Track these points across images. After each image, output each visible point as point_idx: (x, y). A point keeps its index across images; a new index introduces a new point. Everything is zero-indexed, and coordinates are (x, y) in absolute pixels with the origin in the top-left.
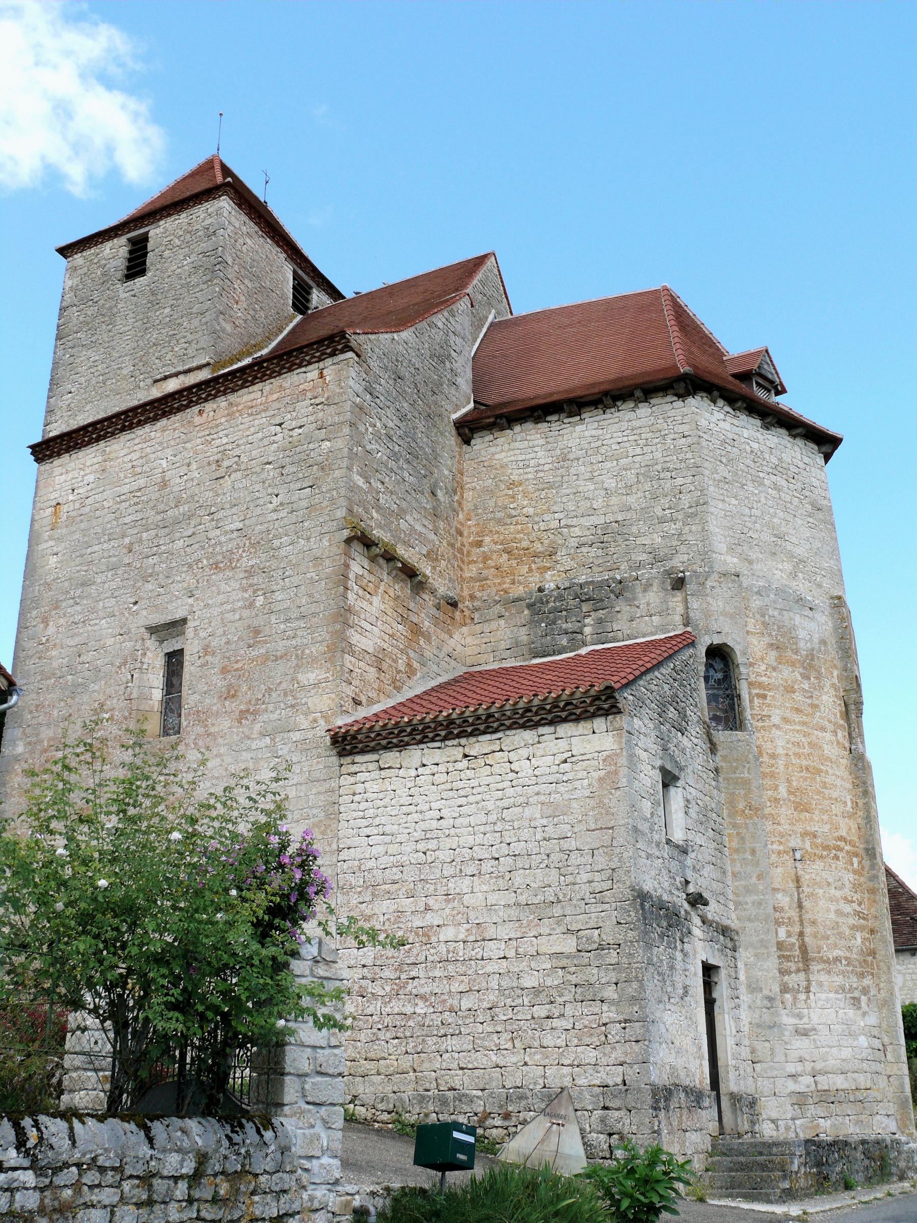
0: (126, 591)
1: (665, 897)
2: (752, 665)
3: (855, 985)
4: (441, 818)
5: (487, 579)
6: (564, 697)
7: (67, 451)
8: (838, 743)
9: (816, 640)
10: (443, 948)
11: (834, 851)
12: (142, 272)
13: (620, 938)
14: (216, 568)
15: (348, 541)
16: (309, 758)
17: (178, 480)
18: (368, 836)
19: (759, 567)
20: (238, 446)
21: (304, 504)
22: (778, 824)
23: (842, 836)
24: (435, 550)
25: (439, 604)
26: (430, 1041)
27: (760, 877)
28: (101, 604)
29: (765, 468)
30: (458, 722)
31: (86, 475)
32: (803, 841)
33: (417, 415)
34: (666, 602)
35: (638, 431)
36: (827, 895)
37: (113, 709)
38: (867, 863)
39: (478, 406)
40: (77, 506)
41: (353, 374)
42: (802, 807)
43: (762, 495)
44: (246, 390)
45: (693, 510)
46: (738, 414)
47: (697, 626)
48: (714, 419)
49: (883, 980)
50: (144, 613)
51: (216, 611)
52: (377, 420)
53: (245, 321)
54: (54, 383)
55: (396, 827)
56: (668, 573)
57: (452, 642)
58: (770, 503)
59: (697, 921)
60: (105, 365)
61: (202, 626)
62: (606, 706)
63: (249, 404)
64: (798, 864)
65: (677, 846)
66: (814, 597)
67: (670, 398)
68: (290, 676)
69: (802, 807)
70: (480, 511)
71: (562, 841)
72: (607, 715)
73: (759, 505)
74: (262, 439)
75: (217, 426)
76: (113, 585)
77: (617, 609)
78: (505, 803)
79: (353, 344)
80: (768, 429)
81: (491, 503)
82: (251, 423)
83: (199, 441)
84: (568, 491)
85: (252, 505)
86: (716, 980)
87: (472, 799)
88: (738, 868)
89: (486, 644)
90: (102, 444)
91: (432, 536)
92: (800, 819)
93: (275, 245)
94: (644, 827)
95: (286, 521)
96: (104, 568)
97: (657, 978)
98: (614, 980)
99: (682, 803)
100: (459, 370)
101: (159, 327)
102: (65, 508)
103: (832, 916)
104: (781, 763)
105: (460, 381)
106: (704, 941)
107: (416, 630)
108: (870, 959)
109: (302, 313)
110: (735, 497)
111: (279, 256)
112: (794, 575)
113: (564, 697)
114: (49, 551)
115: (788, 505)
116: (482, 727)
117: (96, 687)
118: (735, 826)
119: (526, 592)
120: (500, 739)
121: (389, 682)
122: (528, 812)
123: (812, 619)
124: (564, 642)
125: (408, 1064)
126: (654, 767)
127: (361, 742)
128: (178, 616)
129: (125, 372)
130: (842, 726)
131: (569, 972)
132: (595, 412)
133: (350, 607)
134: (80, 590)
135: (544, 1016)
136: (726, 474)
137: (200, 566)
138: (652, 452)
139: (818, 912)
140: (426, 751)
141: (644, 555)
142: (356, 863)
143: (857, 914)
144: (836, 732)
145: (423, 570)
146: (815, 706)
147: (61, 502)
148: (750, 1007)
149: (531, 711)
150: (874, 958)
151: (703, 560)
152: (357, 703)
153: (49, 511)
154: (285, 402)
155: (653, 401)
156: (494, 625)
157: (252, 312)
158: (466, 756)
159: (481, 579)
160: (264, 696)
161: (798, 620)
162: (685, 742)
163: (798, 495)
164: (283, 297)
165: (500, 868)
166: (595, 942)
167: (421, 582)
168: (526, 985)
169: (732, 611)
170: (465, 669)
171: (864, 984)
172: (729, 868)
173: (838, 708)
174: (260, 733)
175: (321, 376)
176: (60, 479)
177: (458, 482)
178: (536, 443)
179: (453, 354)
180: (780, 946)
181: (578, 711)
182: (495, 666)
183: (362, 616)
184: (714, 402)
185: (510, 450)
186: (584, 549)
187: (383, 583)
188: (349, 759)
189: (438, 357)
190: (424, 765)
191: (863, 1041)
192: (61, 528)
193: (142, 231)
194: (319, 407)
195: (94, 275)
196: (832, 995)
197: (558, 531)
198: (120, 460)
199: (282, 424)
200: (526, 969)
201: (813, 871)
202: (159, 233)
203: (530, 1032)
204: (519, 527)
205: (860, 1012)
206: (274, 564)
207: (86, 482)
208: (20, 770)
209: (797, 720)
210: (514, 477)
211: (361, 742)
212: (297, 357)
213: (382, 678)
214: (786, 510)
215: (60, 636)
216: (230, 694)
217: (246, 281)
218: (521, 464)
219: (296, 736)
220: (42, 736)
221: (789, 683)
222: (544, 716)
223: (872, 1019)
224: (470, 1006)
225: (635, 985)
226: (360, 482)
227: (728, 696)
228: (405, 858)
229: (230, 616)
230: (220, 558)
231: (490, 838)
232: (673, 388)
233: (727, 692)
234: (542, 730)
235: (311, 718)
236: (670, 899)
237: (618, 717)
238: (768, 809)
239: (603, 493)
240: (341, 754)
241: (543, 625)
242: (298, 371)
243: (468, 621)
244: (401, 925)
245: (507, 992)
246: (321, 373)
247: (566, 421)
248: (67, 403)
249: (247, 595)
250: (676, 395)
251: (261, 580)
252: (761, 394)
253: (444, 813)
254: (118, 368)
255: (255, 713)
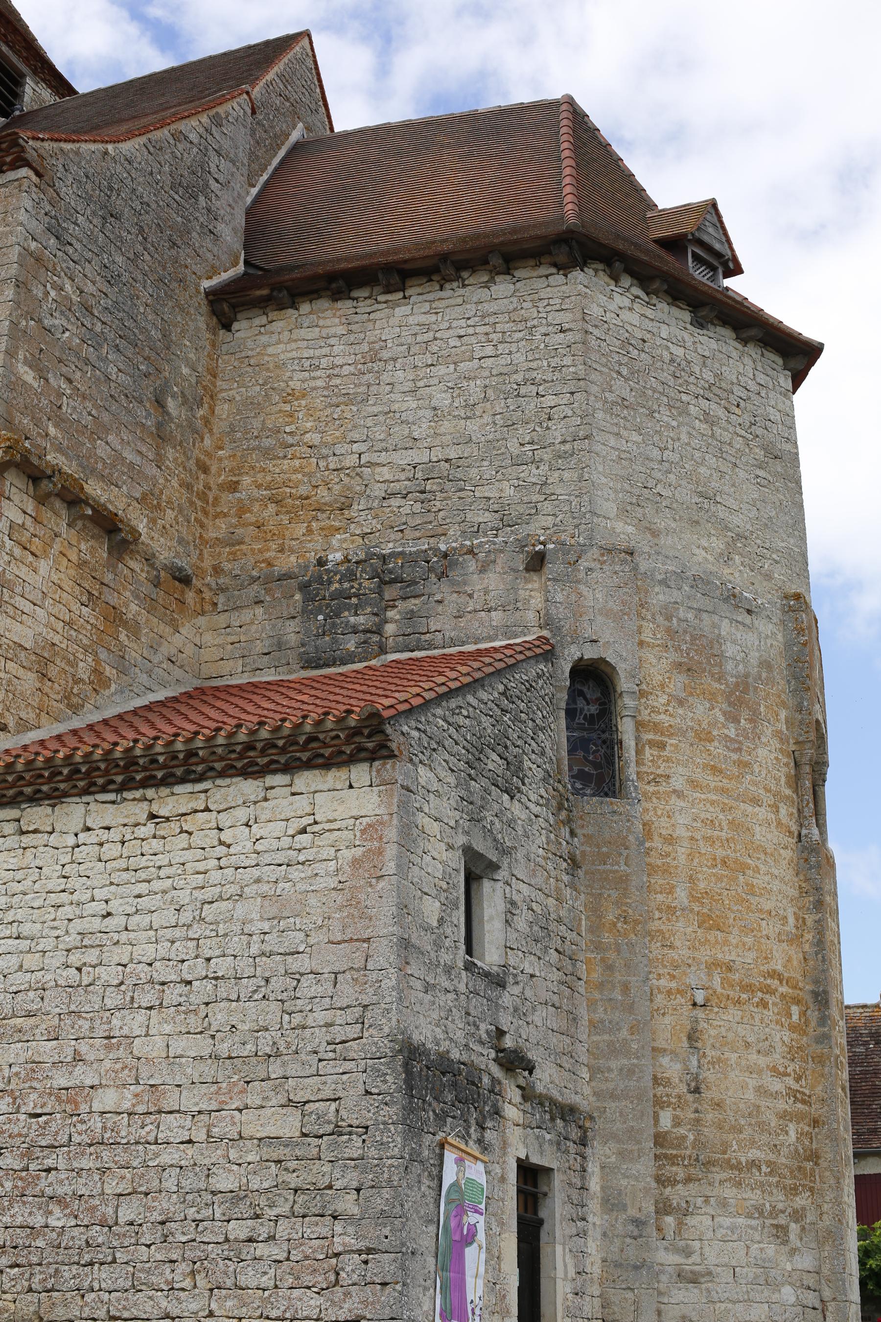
1: (455, 1055)
2: (642, 694)
3: (780, 1206)
4: (109, 914)
5: (241, 543)
6: (308, 728)
8: (779, 823)
9: (754, 662)
10: (96, 1123)
11: (760, 994)
13: (368, 1118)
19: (669, 542)
22: (671, 947)
23: (774, 971)
24: (157, 492)
25: (158, 577)
26: (67, 1272)
27: (632, 1030)
29: (692, 388)
30: (141, 761)
32: (709, 975)
33: (140, 277)
34: (515, 590)
35: (492, 320)
36: (744, 1062)
38: (813, 1015)
41: (28, 204)
42: (711, 922)
43: (684, 429)
45: (568, 447)
46: (654, 300)
47: (559, 629)
48: (613, 307)
49: (827, 1199)
52: (66, 280)
55: (38, 926)
56: (521, 545)
58: (695, 443)
59: (514, 1094)
62: (370, 745)
64: (700, 1013)
65: (487, 975)
66: (756, 593)
67: (544, 270)
69: (711, 922)
70: (239, 435)
71: (290, 959)
72: (373, 760)
73: (677, 444)
77: (438, 597)
78: (209, 893)
79: (31, 155)
80: (702, 326)
81: (256, 424)
84: (376, 409)
86: (545, 1189)
87: (157, 885)
88: (600, 1014)
89: (236, 646)
92: (707, 940)
94: (425, 941)
97: (428, 1183)
98: (355, 1184)
99: (501, 906)
100: (222, 212)
103: (750, 1095)
104: (682, 853)
105: (221, 228)
106: (525, 1127)
107: (115, 617)
108: (809, 1165)
110: (638, 430)
112: (726, 558)
113: (308, 728)
115: (726, 448)
116: (179, 772)
118: (598, 947)
119: (299, 566)
120: (206, 791)
121: (58, 697)
122: (240, 910)
123: (750, 627)
124: (351, 646)
125: (32, 1309)
126: (450, 847)
130: (787, 797)
131: (286, 1169)
132: (427, 287)
135: (242, 1237)
136: (626, 393)
138: (510, 353)
139: (727, 1088)
140: (93, 806)
141: (487, 514)
143: (793, 1094)
144: (777, 808)
146: (744, 765)
148: (604, 1234)
149: (254, 748)
150: (816, 1164)
151: (577, 526)
155: (518, 274)
156: (246, 615)
158: (152, 816)
159: (233, 541)
161: (725, 628)
162: (517, 809)
163: (743, 433)
165: (193, 998)
166: (329, 1122)
167: (124, 541)
168: (221, 1187)
169: (616, 608)
170: (197, 683)
171: (796, 1206)
172: (583, 1012)
173: (784, 770)
177: (205, 388)
178: (332, 331)
179: (214, 185)
180: (660, 1139)
181: (327, 752)
183: (18, 590)
184: (616, 279)
185: (291, 340)
186: (395, 502)
190: (89, 829)
191: (788, 1294)
196: (741, 1221)
197: (356, 471)
200: (221, 1161)
201: (722, 1024)
203: (221, 1262)
204: (297, 463)
205: (787, 1248)
209: (713, 785)
210: (295, 384)
213: (46, 689)
214: (721, 454)
218: (307, 364)
221: (704, 725)
222: (275, 758)
223: (806, 1261)
224: (132, 1217)
225: (386, 1193)
226: (29, 376)
227: (604, 742)
228: (49, 977)
231: (182, 949)
232: (550, 253)
233: (604, 736)
234: (270, 780)
236: (465, 1058)
237: (390, 762)
238: (657, 923)
239: (429, 414)
241: (320, 617)
243: (208, 607)
244: (35, 1084)
245: (189, 1197)
247: (381, 298)
250: (555, 265)
252: (699, 274)
253: (113, 906)
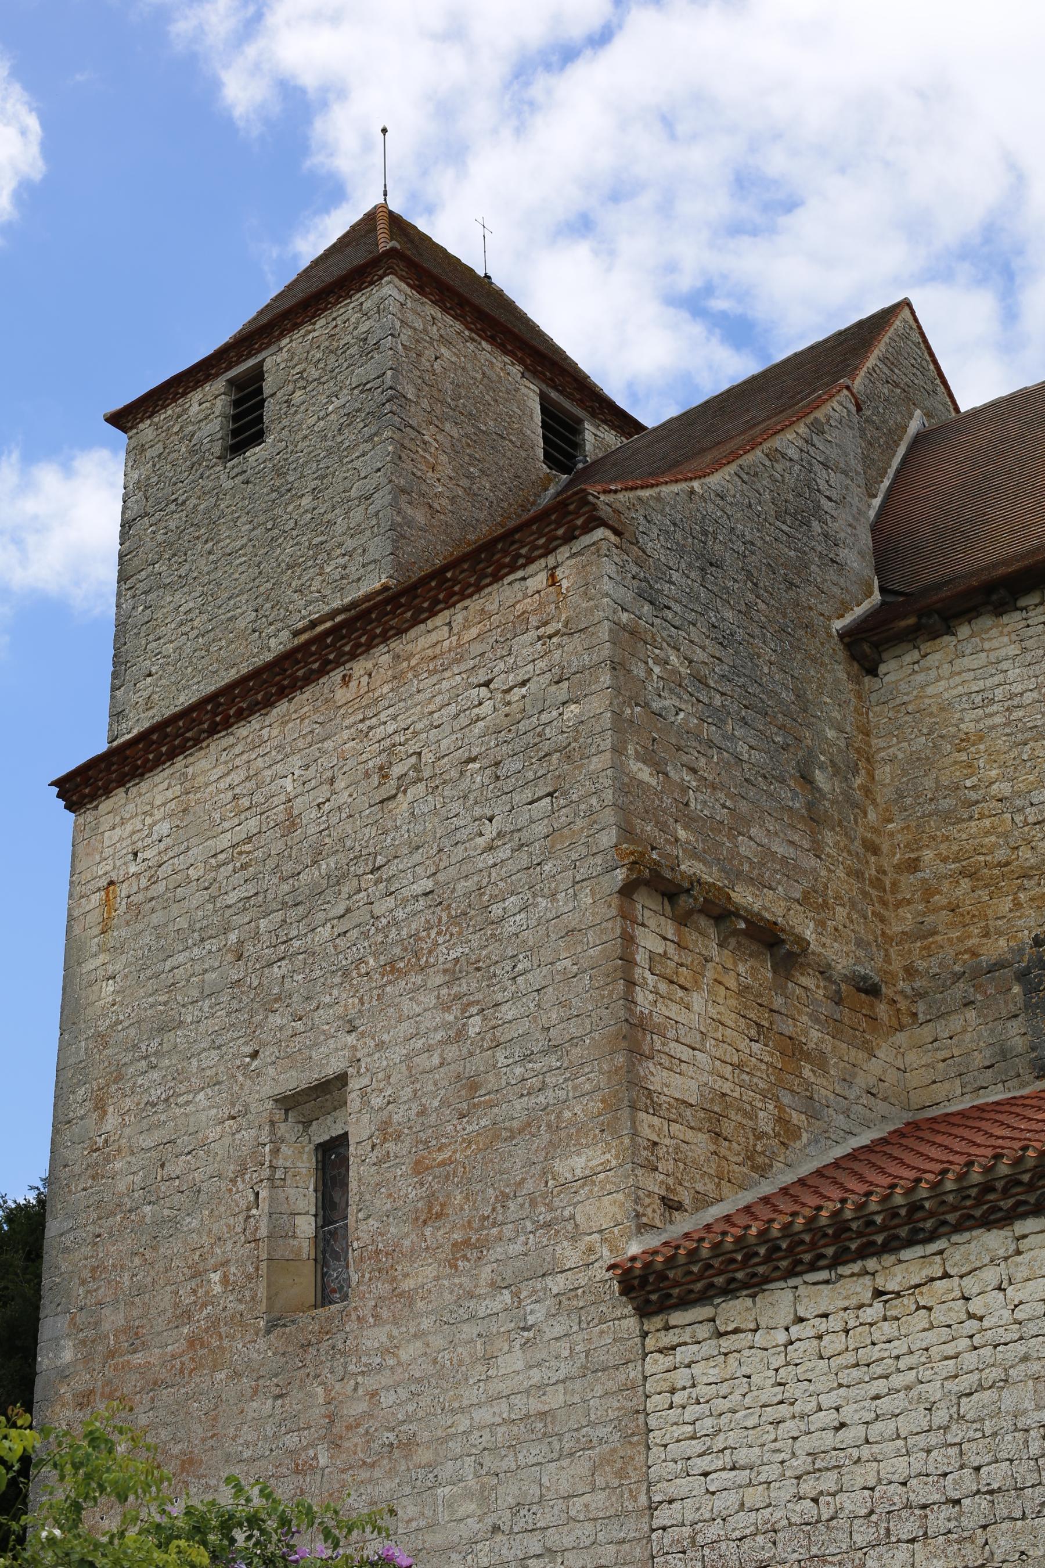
0: (236, 1035)
4: (843, 1425)
5: (934, 933)
7: (121, 783)
12: (258, 438)
14: (392, 972)
15: (627, 891)
16: (584, 1325)
17: (314, 814)
18: (705, 1474)
20: (416, 734)
21: (541, 829)
24: (821, 887)
28: (194, 1062)
30: (854, 1226)
31: (155, 824)
33: (757, 631)
37: (226, 1263)
39: (890, 599)
40: (144, 882)
41: (610, 569)
44: (422, 626)
50: (271, 1071)
51: (397, 1053)
52: (670, 651)
53: (453, 500)
54: (120, 662)
55: (757, 1450)
57: (875, 1066)
60: (205, 617)
61: (374, 1086)
63: (430, 652)
68: (538, 1167)
74: (456, 716)
75: (376, 701)
76: (213, 1024)
78: (965, 1383)
79: (605, 512)
81: (929, 783)
82: (432, 691)
83: (346, 734)
85: (446, 843)
87: (897, 1381)
90: (180, 762)
91: (810, 862)
93: (498, 352)
95: (511, 866)
96: (195, 993)
101: (295, 533)
102: (124, 890)
107: (793, 1050)
109: (566, 470)
111: (509, 370)
114: (101, 973)
117: (195, 1224)
120: (941, 1252)
121: (740, 1159)
122: (1009, 1399)
127: (677, 1284)
128: (333, 1068)
129: (241, 624)
133: (641, 1019)
134: (158, 1040)
137: (363, 971)
140: (802, 1290)
142: (687, 1531)
145: (798, 930)
147: (115, 879)
149: (993, 1189)
152: (671, 1205)
153: (96, 898)
154: (491, 641)
156: (956, 1023)
157: (465, 482)
159: (924, 933)
160: (494, 1209)
164: (525, 444)
167: (790, 954)
170: (908, 1116)
174: (493, 1284)
175: (553, 581)
176: (110, 837)
177: (858, 751)
178: (1002, 653)
182: (965, 1104)
185: (953, 674)
187: (709, 965)
188: (657, 1321)
189: (794, 516)
190: (801, 1320)
192: (118, 927)
193: (251, 362)
194: (554, 640)
195: (175, 455)
198: (211, 788)
199: (490, 681)
202: (275, 362)
204: (987, 822)
206: (494, 950)
207: (155, 837)
208: (69, 1396)
210: (967, 727)
211: (677, 1284)
212: (505, 552)
213: (723, 1152)
215: (127, 1131)
216: (432, 1213)
217: (447, 426)
218: (978, 699)
219: (558, 1284)
220: (106, 1326)
222: (1022, 1198)
226: (644, 773)
229: (423, 1061)
230: (397, 951)
235: (582, 1246)
240: (644, 1312)
242: (511, 578)
243: (906, 1020)
246: (553, 576)
248: (146, 694)
249: (451, 1018)
251: (474, 985)
253: (848, 1413)
254: (230, 619)
255: (481, 1246)
